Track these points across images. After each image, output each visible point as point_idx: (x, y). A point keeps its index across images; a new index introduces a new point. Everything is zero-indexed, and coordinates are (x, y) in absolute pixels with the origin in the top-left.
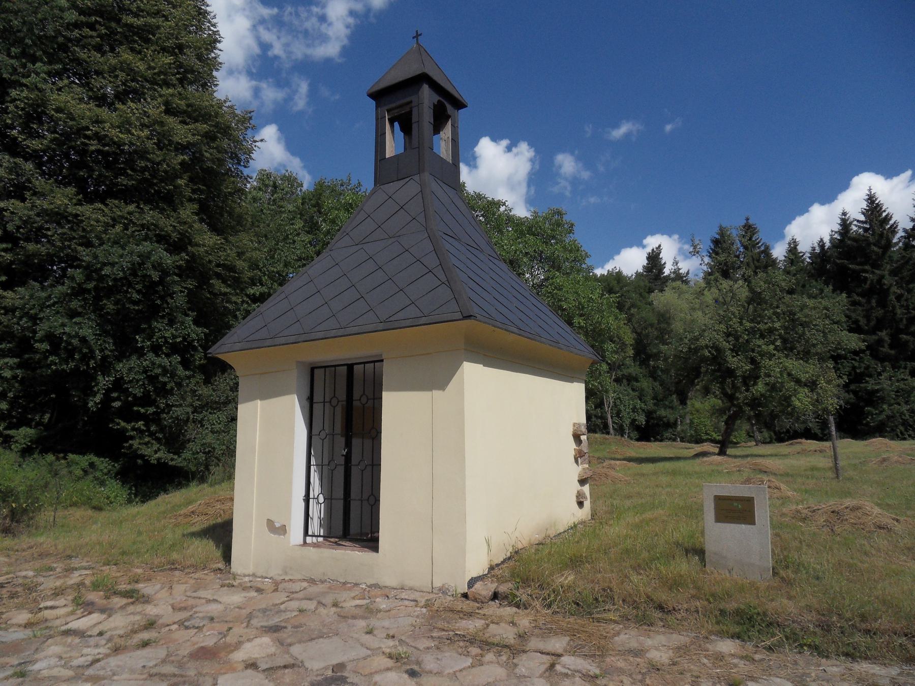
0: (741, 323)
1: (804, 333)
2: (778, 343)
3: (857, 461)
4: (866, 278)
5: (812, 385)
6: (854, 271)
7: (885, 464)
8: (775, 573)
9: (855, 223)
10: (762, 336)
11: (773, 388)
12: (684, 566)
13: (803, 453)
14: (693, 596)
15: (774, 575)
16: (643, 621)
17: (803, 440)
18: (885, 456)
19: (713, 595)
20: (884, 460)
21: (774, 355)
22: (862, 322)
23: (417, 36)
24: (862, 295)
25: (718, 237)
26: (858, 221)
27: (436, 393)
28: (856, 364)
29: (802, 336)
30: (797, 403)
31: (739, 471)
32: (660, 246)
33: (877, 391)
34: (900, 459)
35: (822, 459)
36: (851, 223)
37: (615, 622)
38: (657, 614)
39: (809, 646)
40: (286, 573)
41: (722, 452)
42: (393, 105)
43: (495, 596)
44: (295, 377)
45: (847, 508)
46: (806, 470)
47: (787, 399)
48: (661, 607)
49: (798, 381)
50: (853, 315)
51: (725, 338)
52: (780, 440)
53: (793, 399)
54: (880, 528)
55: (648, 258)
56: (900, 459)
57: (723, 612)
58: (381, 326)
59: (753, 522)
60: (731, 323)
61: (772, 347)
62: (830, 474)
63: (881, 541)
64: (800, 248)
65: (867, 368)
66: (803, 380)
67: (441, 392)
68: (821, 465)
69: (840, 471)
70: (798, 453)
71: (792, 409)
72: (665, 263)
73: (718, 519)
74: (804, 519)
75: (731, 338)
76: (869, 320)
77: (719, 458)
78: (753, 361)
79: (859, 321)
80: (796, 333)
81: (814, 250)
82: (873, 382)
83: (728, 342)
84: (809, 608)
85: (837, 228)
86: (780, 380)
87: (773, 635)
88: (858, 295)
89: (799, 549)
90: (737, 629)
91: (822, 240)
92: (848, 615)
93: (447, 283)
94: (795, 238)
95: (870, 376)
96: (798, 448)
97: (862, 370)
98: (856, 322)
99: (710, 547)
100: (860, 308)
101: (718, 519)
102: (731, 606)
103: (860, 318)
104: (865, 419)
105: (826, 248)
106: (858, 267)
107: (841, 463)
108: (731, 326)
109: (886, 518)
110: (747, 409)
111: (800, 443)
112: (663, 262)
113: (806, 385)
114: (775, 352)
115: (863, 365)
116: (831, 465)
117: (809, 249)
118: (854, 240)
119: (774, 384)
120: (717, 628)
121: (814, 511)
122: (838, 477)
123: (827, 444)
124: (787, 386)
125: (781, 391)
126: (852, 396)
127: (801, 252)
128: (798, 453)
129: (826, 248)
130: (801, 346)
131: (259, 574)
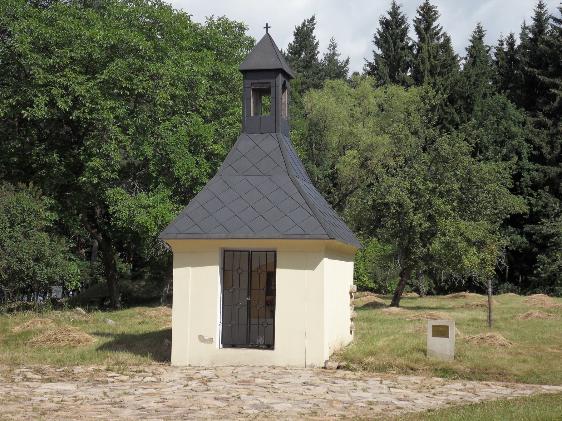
0: (425, 184)
1: (477, 195)
2: (455, 204)
3: (509, 316)
4: (555, 95)
5: (480, 245)
6: (543, 83)
7: (529, 318)
8: (455, 358)
9: (551, 21)
10: (441, 195)
11: (447, 246)
12: (419, 355)
13: (467, 307)
14: (424, 365)
15: (455, 359)
16: (406, 373)
17: (467, 294)
18: (530, 312)
19: (433, 364)
20: (529, 315)
21: (450, 214)
22: (546, 149)
23: (267, 27)
24: (548, 115)
25: (389, 17)
26: (555, 20)
27: (308, 271)
28: (533, 201)
29: (475, 197)
30: (466, 262)
31: (419, 320)
32: (313, 19)
33: (553, 235)
34: (540, 315)
35: (481, 313)
36: (547, 19)
37: (395, 374)
38: (411, 371)
39: (467, 378)
40: (213, 364)
41: (395, 303)
42: (257, 81)
43: (338, 368)
44: (218, 256)
45: (488, 336)
46: (468, 321)
47: (459, 257)
48: (412, 369)
49: (468, 241)
50: (537, 140)
51: (409, 195)
52: (441, 291)
53: (463, 257)
54: (502, 345)
55: (296, 34)
56: (540, 315)
57: (436, 369)
58: (282, 236)
59: (448, 337)
60: (414, 180)
61: (449, 207)
62: (486, 324)
63: (500, 350)
64: (486, 41)
65: (545, 206)
66: (473, 240)
67: (311, 271)
68: (480, 317)
69: (492, 323)
70: (462, 307)
71: (461, 266)
72: (317, 44)
73: (433, 336)
74: (467, 342)
75: (413, 197)
76: (552, 148)
77: (394, 309)
78: (430, 218)
79: (542, 148)
80: (471, 194)
81: (502, 44)
82: (549, 224)
83: (411, 200)
84: (468, 367)
85: (531, 23)
86: (453, 240)
87: (455, 376)
88: (545, 115)
89: (465, 350)
90: (442, 374)
91: (511, 37)
92: (481, 368)
93: (313, 215)
94: (481, 25)
95: (547, 216)
96: (461, 302)
97: (540, 208)
98: (538, 148)
99: (429, 347)
100: (545, 132)
101: (433, 336)
102: (440, 367)
103: (544, 145)
104: (536, 268)
105: (516, 47)
106: (547, 80)
107: (494, 316)
108: (415, 184)
109: (506, 342)
110: (421, 263)
111: (465, 296)
112: (315, 42)
113: (474, 244)
114: (452, 212)
115: (541, 203)
116: (486, 318)
117: (496, 43)
118: (548, 44)
119: (448, 243)
120: (434, 375)
121: (472, 338)
122: (490, 326)
123: (485, 298)
124: (459, 245)
125: (453, 250)
126: (525, 239)
127: (487, 46)
128: (462, 307)
129: (516, 47)
130: (474, 207)
131: (193, 365)
